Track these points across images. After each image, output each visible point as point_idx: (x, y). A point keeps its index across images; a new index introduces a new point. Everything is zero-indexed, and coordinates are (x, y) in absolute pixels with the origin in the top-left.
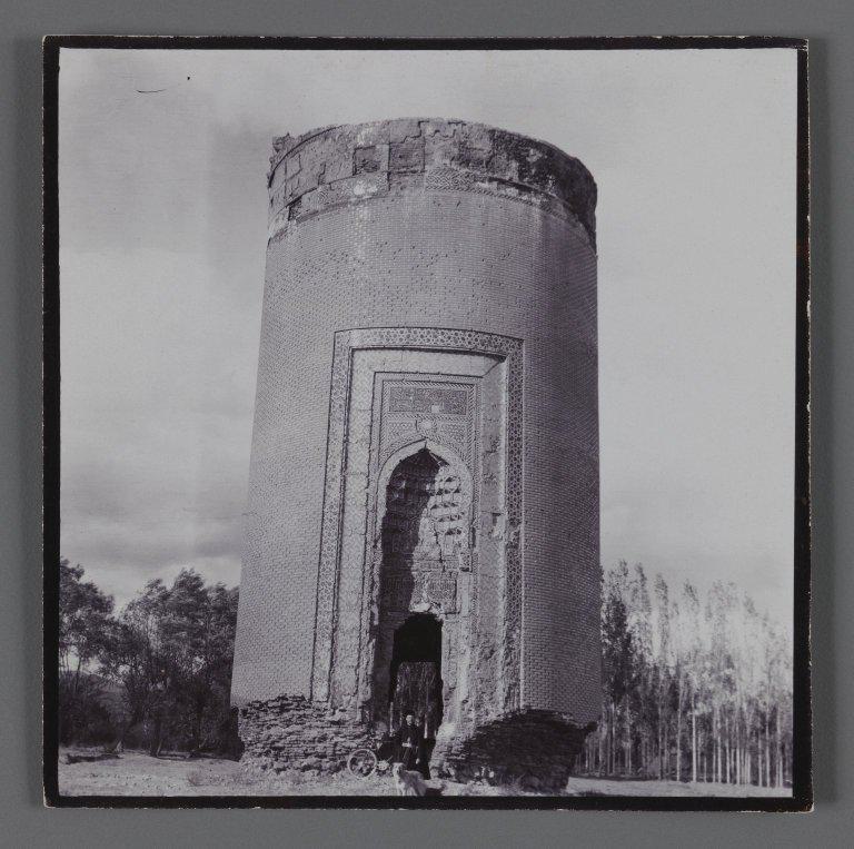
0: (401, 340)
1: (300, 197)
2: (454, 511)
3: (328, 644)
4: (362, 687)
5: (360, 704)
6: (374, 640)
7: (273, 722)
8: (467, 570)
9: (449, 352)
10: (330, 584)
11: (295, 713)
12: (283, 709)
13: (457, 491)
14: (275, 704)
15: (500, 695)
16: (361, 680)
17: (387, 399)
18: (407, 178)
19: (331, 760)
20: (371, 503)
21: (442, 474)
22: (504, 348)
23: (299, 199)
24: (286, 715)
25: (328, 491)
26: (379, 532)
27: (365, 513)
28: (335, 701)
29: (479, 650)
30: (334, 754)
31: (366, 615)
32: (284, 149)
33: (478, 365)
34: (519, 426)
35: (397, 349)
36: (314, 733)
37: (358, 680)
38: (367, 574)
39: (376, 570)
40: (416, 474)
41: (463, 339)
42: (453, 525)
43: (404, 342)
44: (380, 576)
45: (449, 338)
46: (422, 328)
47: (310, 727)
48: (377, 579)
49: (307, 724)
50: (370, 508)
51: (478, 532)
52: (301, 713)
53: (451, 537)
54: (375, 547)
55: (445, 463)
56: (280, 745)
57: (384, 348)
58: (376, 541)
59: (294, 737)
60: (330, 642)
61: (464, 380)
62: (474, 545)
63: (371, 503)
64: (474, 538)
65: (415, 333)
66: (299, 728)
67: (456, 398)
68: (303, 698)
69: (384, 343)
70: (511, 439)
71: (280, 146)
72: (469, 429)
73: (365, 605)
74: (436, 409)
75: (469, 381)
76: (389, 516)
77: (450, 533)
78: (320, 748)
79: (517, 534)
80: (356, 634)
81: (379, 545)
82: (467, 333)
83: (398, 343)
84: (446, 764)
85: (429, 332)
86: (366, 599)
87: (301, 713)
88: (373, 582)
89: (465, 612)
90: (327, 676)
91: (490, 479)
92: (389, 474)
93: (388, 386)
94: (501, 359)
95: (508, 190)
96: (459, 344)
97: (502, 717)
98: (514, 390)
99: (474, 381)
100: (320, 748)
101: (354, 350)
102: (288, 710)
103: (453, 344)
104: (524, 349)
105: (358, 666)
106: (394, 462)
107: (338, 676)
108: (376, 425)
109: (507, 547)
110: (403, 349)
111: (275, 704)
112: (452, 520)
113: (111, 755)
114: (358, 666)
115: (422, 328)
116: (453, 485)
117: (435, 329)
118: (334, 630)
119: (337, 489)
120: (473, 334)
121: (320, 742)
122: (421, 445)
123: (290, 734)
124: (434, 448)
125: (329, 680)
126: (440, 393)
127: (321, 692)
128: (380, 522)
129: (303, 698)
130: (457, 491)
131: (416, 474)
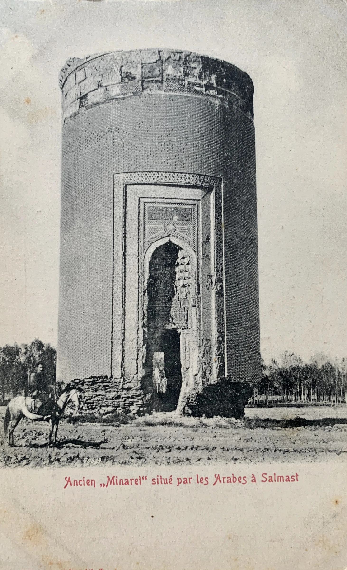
0: (154, 179)
1: (87, 94)
2: (186, 274)
3: (120, 347)
4: (140, 369)
5: (140, 379)
6: (146, 345)
7: (87, 390)
8: (195, 306)
9: (181, 186)
10: (119, 316)
11: (101, 384)
12: (94, 383)
13: (188, 264)
14: (89, 380)
15: (215, 372)
16: (139, 366)
17: (147, 213)
18: (153, 84)
19: (122, 408)
20: (141, 271)
21: (180, 254)
22: (211, 183)
23: (85, 96)
24: (96, 386)
25: (115, 265)
26: (146, 287)
27: (138, 276)
28: (125, 377)
29: (202, 348)
30: (124, 405)
31: (141, 331)
32: (74, 65)
33: (198, 193)
34: (221, 227)
35: (151, 184)
36: (112, 395)
37: (137, 366)
38: (141, 310)
39: (145, 308)
40: (167, 255)
41: (189, 178)
42: (186, 282)
43: (156, 180)
44: (147, 310)
45: (181, 178)
46: (166, 172)
47: (110, 391)
48: (146, 312)
49: (108, 390)
50: (140, 274)
51: (201, 286)
52: (105, 384)
53: (184, 289)
54: (144, 295)
55: (181, 249)
56: (91, 401)
57: (144, 184)
58: (144, 292)
59: (100, 397)
60: (121, 346)
61: (189, 202)
62: (199, 293)
63: (141, 271)
64: (199, 289)
65: (162, 175)
66: (103, 392)
67: (186, 216)
68: (106, 377)
69: (144, 180)
70: (217, 234)
71: (71, 64)
72: (194, 230)
73: (140, 326)
74: (175, 218)
75: (193, 203)
76: (151, 277)
77: (184, 286)
78: (116, 402)
79: (222, 286)
80: (135, 341)
81: (146, 294)
82: (191, 175)
83: (152, 181)
84: (187, 408)
85: (170, 175)
86: (141, 324)
87: (105, 384)
88: (144, 314)
89: (194, 328)
90: (120, 365)
91: (206, 256)
92: (150, 255)
93: (147, 206)
94: (209, 190)
95: (211, 91)
96: (187, 181)
97: (216, 382)
98: (218, 208)
99: (196, 202)
100: (116, 402)
101: (126, 185)
102: (97, 383)
103: (183, 181)
104: (222, 184)
105: (138, 359)
106: (149, 254)
107: (126, 365)
108: (142, 228)
109: (216, 293)
110: (155, 184)
111: (89, 380)
112: (185, 279)
113: (217, 59)
114: (138, 359)
115: (166, 172)
116: (186, 260)
117: (174, 173)
118: (123, 340)
119: (121, 263)
120: (195, 175)
121: (116, 399)
122: (165, 241)
123: (97, 396)
124: (175, 241)
125: (122, 367)
126: (176, 209)
127: (117, 373)
128: (146, 281)
129: (106, 377)
130: (188, 264)
131: (167, 255)
